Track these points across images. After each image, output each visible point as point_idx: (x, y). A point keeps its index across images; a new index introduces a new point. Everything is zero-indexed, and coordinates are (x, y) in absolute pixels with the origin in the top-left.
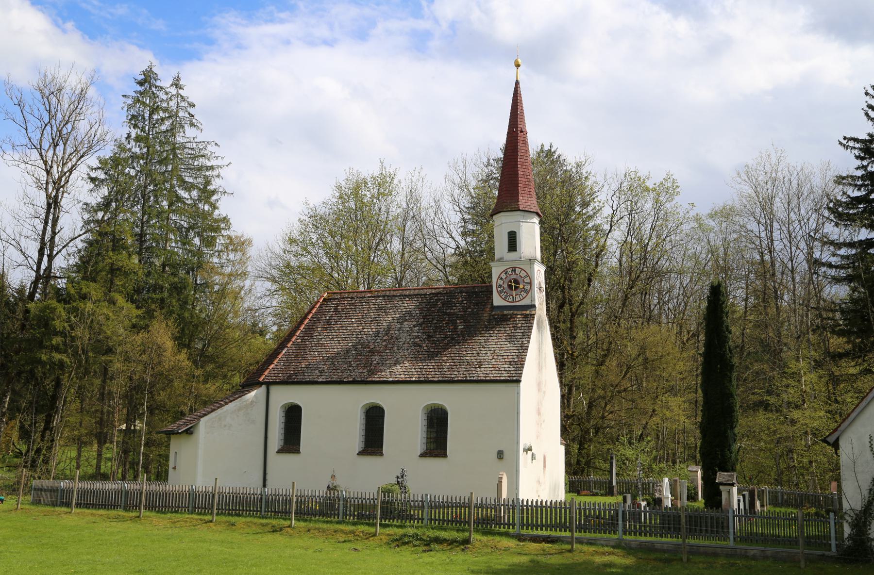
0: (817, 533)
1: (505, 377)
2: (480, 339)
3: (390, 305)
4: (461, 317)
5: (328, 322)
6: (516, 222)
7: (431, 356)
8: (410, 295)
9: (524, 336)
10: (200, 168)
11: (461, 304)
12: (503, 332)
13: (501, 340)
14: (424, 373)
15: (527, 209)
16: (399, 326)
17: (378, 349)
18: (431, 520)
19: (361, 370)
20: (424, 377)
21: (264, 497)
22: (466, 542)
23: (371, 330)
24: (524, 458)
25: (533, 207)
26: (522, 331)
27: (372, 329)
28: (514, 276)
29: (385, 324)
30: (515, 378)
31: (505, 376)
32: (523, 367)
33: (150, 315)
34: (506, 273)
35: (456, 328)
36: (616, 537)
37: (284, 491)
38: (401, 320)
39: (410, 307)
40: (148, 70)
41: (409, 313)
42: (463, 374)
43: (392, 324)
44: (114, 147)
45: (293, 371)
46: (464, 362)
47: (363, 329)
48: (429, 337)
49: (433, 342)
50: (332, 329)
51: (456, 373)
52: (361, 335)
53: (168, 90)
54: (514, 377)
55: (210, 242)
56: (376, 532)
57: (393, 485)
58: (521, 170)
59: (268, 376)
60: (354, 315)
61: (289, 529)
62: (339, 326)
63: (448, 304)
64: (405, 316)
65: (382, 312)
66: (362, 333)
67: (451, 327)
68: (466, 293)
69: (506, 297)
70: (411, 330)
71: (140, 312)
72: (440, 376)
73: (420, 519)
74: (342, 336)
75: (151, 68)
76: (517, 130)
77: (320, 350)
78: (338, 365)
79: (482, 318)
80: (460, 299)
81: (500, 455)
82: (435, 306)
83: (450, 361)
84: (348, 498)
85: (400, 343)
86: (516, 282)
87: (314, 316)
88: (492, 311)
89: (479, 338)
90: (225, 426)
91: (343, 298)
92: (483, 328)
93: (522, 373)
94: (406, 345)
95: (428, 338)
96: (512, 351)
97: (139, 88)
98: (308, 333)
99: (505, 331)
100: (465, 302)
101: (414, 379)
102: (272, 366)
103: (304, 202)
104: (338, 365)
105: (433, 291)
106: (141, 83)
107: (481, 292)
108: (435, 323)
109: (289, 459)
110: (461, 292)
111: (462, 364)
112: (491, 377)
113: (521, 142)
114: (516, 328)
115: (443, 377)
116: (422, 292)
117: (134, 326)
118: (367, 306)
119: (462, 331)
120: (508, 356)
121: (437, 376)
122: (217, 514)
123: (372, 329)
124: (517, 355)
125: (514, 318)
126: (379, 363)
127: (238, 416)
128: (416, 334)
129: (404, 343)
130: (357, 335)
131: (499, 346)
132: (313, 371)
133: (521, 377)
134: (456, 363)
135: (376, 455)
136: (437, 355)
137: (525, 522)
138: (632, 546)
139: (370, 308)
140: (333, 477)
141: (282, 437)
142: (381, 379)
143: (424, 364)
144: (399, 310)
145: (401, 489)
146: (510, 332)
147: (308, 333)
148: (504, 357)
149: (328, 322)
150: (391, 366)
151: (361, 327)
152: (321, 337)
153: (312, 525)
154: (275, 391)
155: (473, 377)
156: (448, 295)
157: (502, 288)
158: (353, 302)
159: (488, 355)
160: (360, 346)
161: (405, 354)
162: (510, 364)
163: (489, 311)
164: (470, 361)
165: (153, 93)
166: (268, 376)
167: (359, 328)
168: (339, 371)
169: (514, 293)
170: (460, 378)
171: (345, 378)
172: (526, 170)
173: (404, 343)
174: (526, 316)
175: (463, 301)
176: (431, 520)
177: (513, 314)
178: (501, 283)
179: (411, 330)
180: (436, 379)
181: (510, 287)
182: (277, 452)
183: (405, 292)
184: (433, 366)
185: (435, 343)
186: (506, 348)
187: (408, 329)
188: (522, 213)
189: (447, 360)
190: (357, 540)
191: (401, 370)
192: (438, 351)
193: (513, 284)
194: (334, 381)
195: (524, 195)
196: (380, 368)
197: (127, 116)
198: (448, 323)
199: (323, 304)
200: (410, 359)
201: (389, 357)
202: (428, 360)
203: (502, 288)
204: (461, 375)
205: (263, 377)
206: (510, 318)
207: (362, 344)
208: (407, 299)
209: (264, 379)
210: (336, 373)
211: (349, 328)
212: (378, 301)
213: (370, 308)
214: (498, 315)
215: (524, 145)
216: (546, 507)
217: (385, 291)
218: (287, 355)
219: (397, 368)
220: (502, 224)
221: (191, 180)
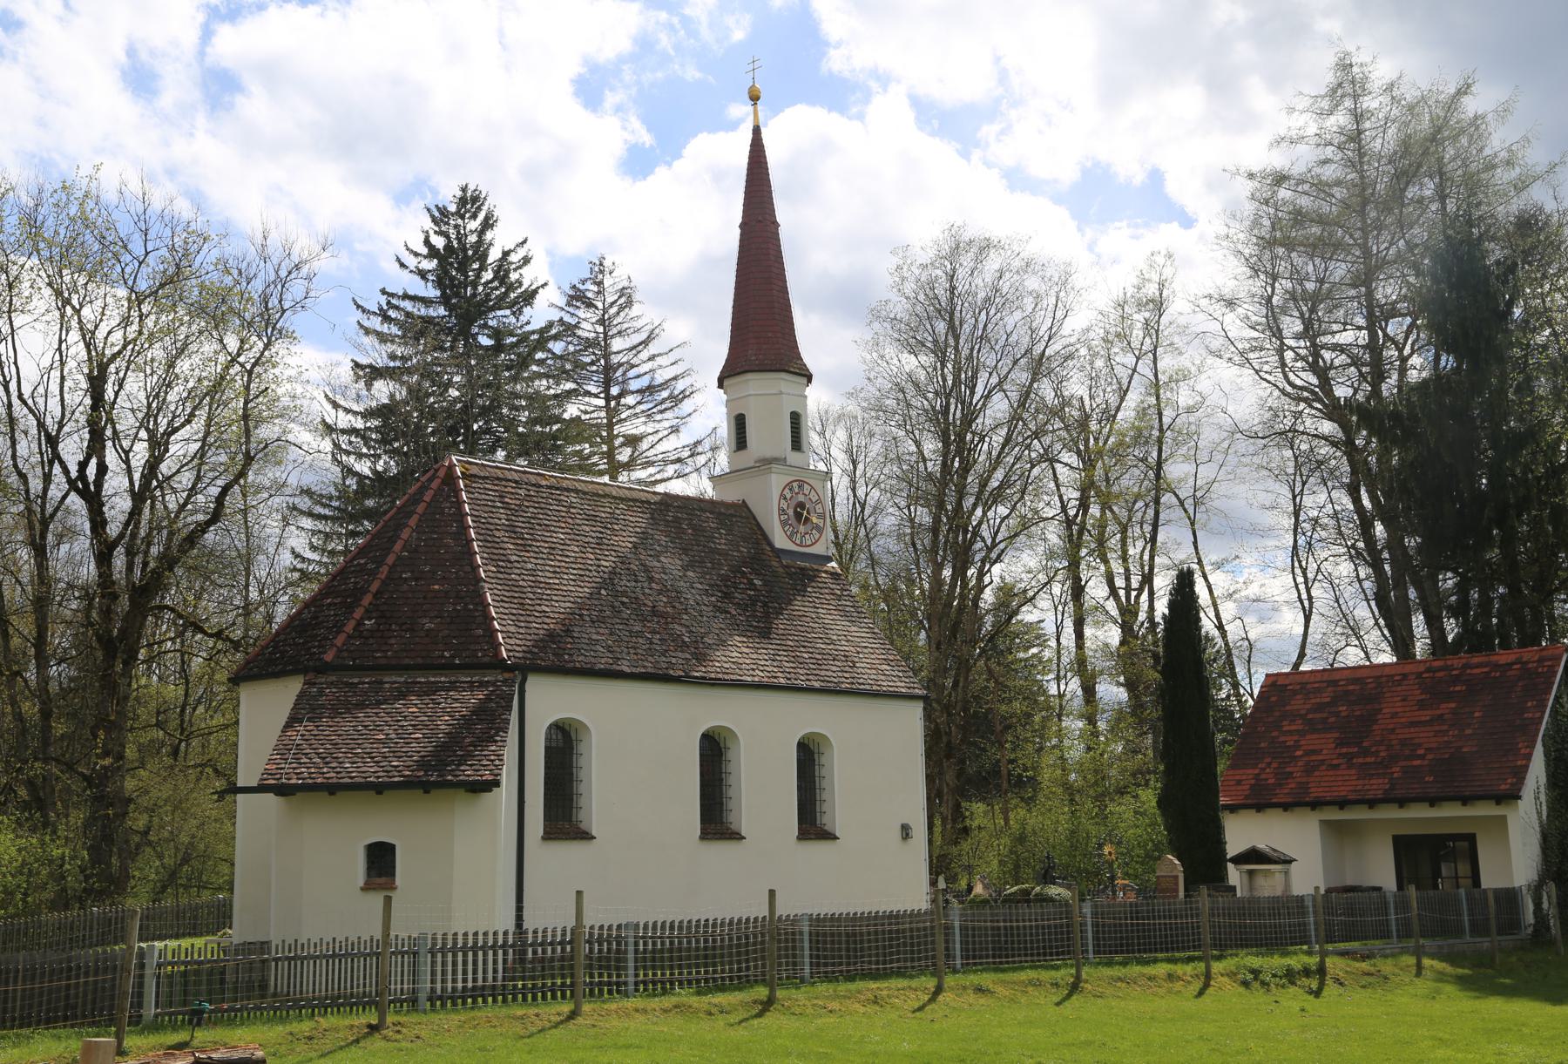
28: (801, 498)
69: (793, 533)
220: (781, 393)
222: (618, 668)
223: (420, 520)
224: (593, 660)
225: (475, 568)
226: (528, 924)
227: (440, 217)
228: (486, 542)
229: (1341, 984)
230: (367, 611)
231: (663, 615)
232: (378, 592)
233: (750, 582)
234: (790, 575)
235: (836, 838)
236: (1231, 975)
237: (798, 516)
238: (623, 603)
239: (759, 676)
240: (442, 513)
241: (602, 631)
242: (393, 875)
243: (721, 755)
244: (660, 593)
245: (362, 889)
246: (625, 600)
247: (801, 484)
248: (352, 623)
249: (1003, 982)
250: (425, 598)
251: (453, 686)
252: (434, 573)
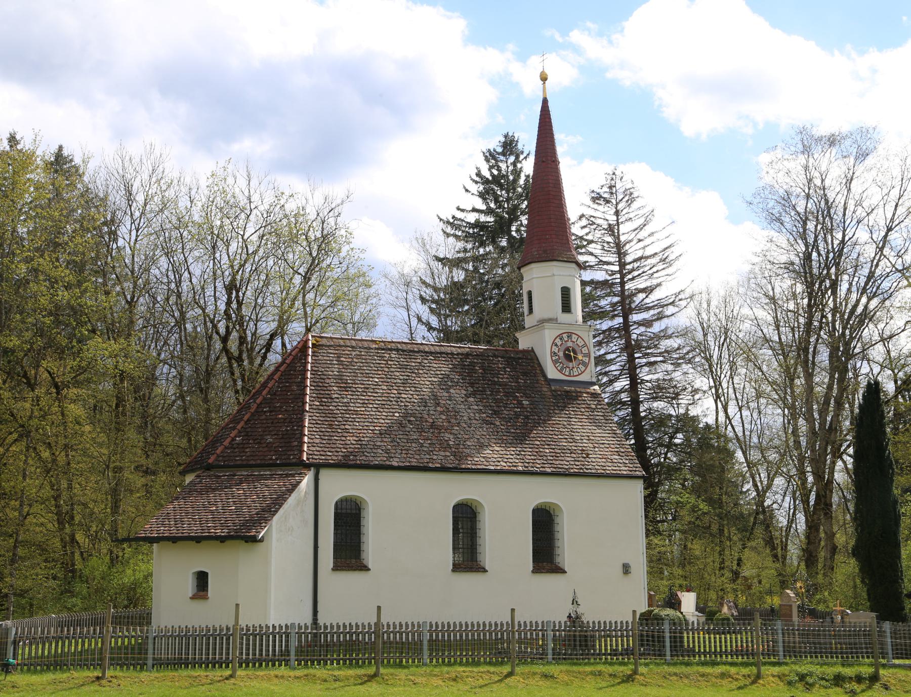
6: (570, 276)
28: (570, 344)
34: (561, 339)
69: (562, 368)
140: (574, 602)
154: (324, 474)
178: (556, 351)
220: (554, 275)
222: (390, 463)
223: (282, 375)
224: (371, 459)
225: (304, 403)
226: (321, 622)
227: (490, 156)
228: (317, 386)
229: (887, 689)
230: (240, 432)
231: (439, 428)
232: (248, 420)
233: (520, 403)
234: (555, 397)
235: (564, 572)
236: (780, 677)
237: (568, 358)
238: (409, 421)
239: (503, 465)
240: (295, 371)
241: (385, 440)
242: (207, 591)
243: (475, 517)
244: (441, 413)
245: (191, 598)
246: (412, 419)
247: (570, 335)
248: (229, 440)
249: (568, 672)
250: (272, 423)
251: (271, 477)
252: (281, 407)
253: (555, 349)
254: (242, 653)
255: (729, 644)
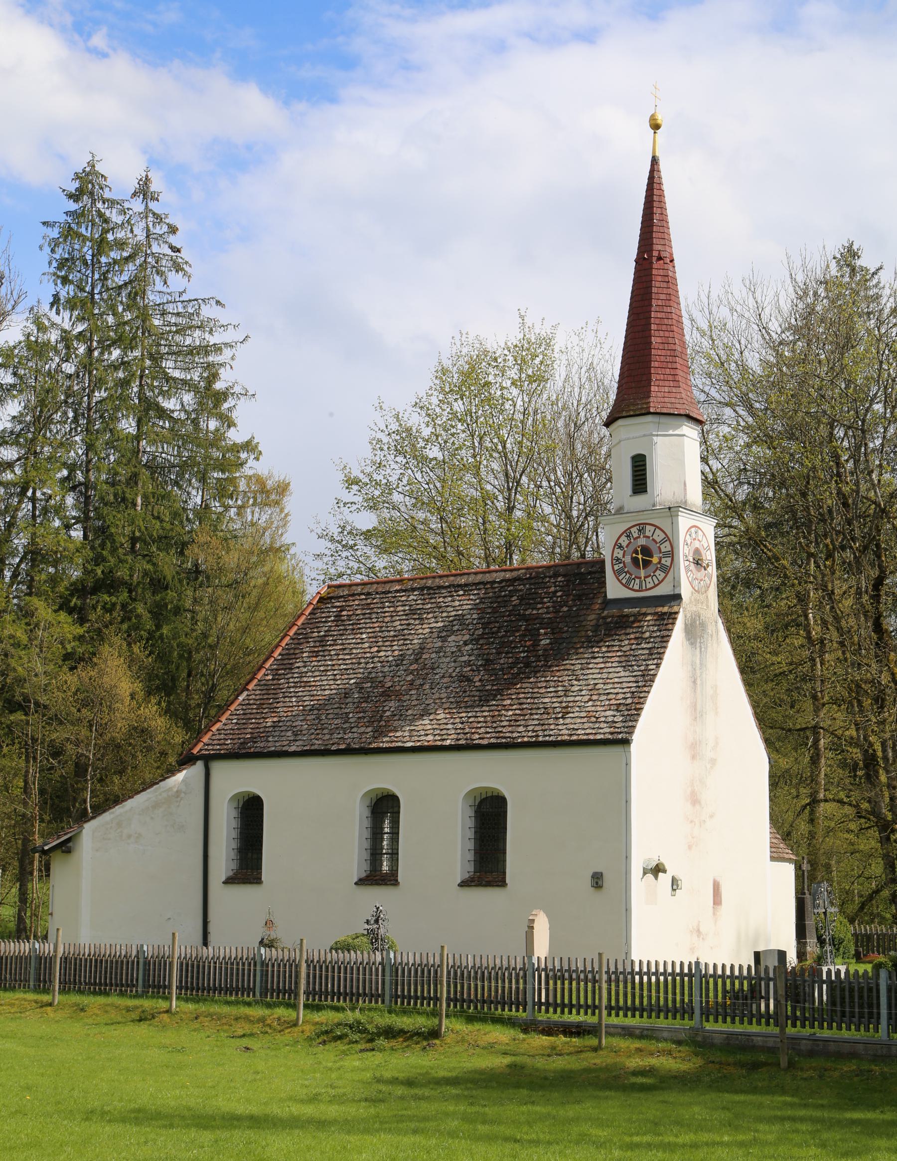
0: (720, 999)
1: (604, 734)
2: (574, 663)
3: (429, 606)
4: (548, 624)
5: (322, 641)
6: (644, 436)
7: (485, 698)
8: (466, 585)
9: (652, 654)
10: (192, 351)
11: (551, 598)
12: (616, 648)
13: (610, 665)
14: (467, 730)
15: (665, 411)
16: (440, 644)
17: (397, 688)
18: (397, 996)
19: (362, 730)
20: (466, 739)
21: (141, 960)
22: (435, 1034)
23: (389, 654)
24: (639, 885)
25: (678, 406)
26: (650, 645)
27: (394, 651)
28: (642, 541)
29: (415, 641)
30: (620, 736)
31: (604, 732)
32: (639, 715)
33: (99, 636)
34: (628, 536)
35: (536, 643)
36: (692, 1023)
37: (240, 950)
38: (444, 634)
39: (464, 607)
40: (88, 169)
41: (460, 618)
42: (533, 731)
43: (428, 641)
44: (25, 324)
45: (251, 733)
46: (539, 708)
47: (378, 651)
48: (488, 662)
49: (493, 672)
50: (326, 653)
51: (521, 729)
52: (373, 662)
53: (126, 205)
54: (620, 733)
55: (224, 491)
56: (298, 1018)
57: (357, 937)
58: (657, 334)
59: (208, 745)
60: (368, 625)
61: (166, 1015)
62: (338, 647)
63: (529, 599)
64: (453, 626)
65: (415, 619)
66: (376, 659)
67: (528, 643)
68: (564, 576)
70: (460, 651)
71: (80, 631)
72: (494, 735)
73: (379, 996)
74: (342, 667)
75: (93, 166)
76: (651, 256)
77: (300, 694)
78: (326, 721)
79: (584, 623)
80: (553, 589)
81: (597, 880)
82: (505, 603)
83: (514, 707)
84: (486, 968)
85: (437, 677)
86: (646, 551)
87: (300, 631)
88: (603, 609)
89: (573, 662)
90: (129, 837)
91: (353, 595)
92: (583, 642)
93: (634, 727)
94: (445, 680)
95: (485, 665)
96: (625, 685)
97: (73, 206)
98: (286, 662)
99: (620, 646)
100: (559, 594)
101: (448, 742)
102: (218, 725)
103: (377, 405)
104: (326, 721)
105: (508, 575)
106: (75, 197)
107: (590, 573)
108: (502, 637)
109: (244, 893)
110: (556, 575)
111: (534, 712)
112: (581, 735)
113: (660, 279)
114: (640, 639)
115: (498, 738)
116: (488, 578)
117: (67, 657)
118: (392, 609)
119: (545, 650)
120: (617, 693)
121: (488, 736)
122: (63, 991)
123: (394, 651)
124: (633, 693)
125: (640, 621)
126: (395, 715)
127: (152, 818)
128: (466, 658)
129: (443, 677)
130: (367, 663)
131: (605, 676)
132: (283, 734)
133: (631, 733)
134: (525, 712)
135: (386, 884)
136: (496, 696)
137: (559, 1001)
138: (716, 1041)
139: (395, 611)
140: (269, 924)
141: (470, 856)
142: (393, 745)
143: (470, 715)
144: (445, 614)
145: (372, 943)
146: (628, 648)
147: (286, 662)
148: (610, 696)
149: (322, 641)
150: (414, 720)
151: (376, 649)
152: (306, 670)
153: (202, 1008)
154: (219, 769)
155: (550, 736)
156: (533, 581)
157: (621, 565)
158: (369, 601)
159: (583, 693)
160: (369, 685)
161: (443, 696)
162: (617, 710)
163: (599, 609)
164: (549, 705)
165: (100, 215)
166: (208, 745)
167: (372, 650)
168: (326, 731)
169: (642, 573)
170: (526, 739)
171: (333, 744)
172: (667, 334)
173: (443, 677)
174: (661, 616)
175: (556, 592)
176: (397, 996)
177: (639, 614)
178: (620, 556)
179: (460, 651)
180: (485, 742)
181: (635, 561)
182: (224, 883)
183: (459, 578)
184: (485, 717)
185: (496, 675)
186: (616, 680)
187: (455, 649)
188: (655, 419)
189: (511, 705)
190: (267, 1033)
191: (429, 727)
192: (498, 689)
193: (640, 556)
194: (316, 750)
195: (661, 383)
196: (396, 723)
197: (50, 263)
198: (524, 636)
199: (318, 608)
200: (446, 706)
201: (413, 703)
202: (478, 706)
203: (621, 565)
204: (530, 734)
205: (200, 745)
206: (633, 622)
207: (372, 681)
208: (461, 593)
209: (201, 750)
210: (320, 736)
211: (354, 651)
212: (412, 597)
213: (395, 611)
214: (613, 617)
215: (665, 285)
216: (723, 976)
217: (427, 578)
218: (246, 704)
219: (423, 722)
220: (620, 441)
221: (176, 374)
247: (641, 527)
253: (619, 553)
254: (853, 1002)
255: (645, 993)
